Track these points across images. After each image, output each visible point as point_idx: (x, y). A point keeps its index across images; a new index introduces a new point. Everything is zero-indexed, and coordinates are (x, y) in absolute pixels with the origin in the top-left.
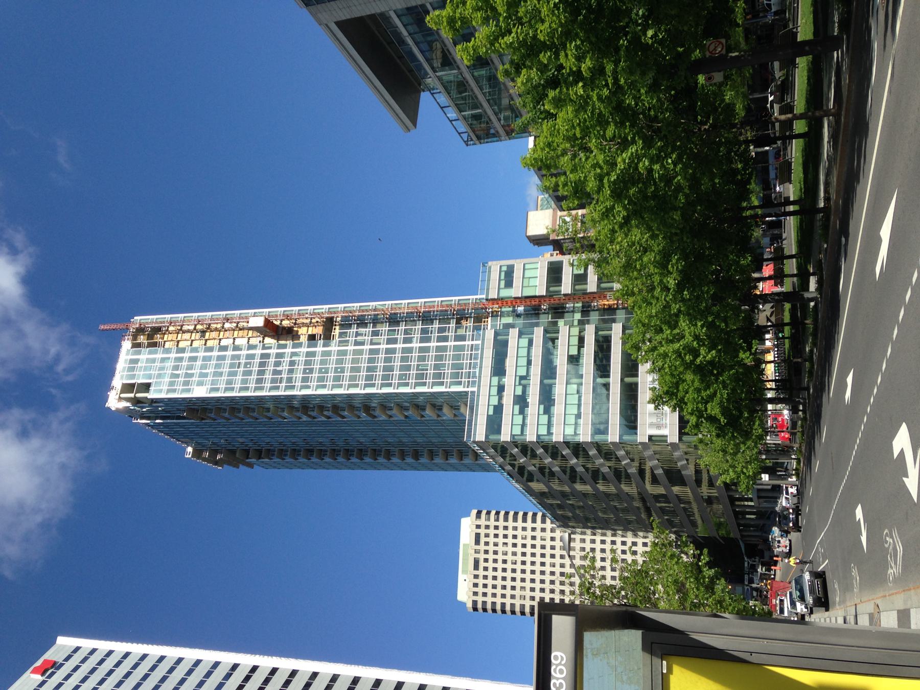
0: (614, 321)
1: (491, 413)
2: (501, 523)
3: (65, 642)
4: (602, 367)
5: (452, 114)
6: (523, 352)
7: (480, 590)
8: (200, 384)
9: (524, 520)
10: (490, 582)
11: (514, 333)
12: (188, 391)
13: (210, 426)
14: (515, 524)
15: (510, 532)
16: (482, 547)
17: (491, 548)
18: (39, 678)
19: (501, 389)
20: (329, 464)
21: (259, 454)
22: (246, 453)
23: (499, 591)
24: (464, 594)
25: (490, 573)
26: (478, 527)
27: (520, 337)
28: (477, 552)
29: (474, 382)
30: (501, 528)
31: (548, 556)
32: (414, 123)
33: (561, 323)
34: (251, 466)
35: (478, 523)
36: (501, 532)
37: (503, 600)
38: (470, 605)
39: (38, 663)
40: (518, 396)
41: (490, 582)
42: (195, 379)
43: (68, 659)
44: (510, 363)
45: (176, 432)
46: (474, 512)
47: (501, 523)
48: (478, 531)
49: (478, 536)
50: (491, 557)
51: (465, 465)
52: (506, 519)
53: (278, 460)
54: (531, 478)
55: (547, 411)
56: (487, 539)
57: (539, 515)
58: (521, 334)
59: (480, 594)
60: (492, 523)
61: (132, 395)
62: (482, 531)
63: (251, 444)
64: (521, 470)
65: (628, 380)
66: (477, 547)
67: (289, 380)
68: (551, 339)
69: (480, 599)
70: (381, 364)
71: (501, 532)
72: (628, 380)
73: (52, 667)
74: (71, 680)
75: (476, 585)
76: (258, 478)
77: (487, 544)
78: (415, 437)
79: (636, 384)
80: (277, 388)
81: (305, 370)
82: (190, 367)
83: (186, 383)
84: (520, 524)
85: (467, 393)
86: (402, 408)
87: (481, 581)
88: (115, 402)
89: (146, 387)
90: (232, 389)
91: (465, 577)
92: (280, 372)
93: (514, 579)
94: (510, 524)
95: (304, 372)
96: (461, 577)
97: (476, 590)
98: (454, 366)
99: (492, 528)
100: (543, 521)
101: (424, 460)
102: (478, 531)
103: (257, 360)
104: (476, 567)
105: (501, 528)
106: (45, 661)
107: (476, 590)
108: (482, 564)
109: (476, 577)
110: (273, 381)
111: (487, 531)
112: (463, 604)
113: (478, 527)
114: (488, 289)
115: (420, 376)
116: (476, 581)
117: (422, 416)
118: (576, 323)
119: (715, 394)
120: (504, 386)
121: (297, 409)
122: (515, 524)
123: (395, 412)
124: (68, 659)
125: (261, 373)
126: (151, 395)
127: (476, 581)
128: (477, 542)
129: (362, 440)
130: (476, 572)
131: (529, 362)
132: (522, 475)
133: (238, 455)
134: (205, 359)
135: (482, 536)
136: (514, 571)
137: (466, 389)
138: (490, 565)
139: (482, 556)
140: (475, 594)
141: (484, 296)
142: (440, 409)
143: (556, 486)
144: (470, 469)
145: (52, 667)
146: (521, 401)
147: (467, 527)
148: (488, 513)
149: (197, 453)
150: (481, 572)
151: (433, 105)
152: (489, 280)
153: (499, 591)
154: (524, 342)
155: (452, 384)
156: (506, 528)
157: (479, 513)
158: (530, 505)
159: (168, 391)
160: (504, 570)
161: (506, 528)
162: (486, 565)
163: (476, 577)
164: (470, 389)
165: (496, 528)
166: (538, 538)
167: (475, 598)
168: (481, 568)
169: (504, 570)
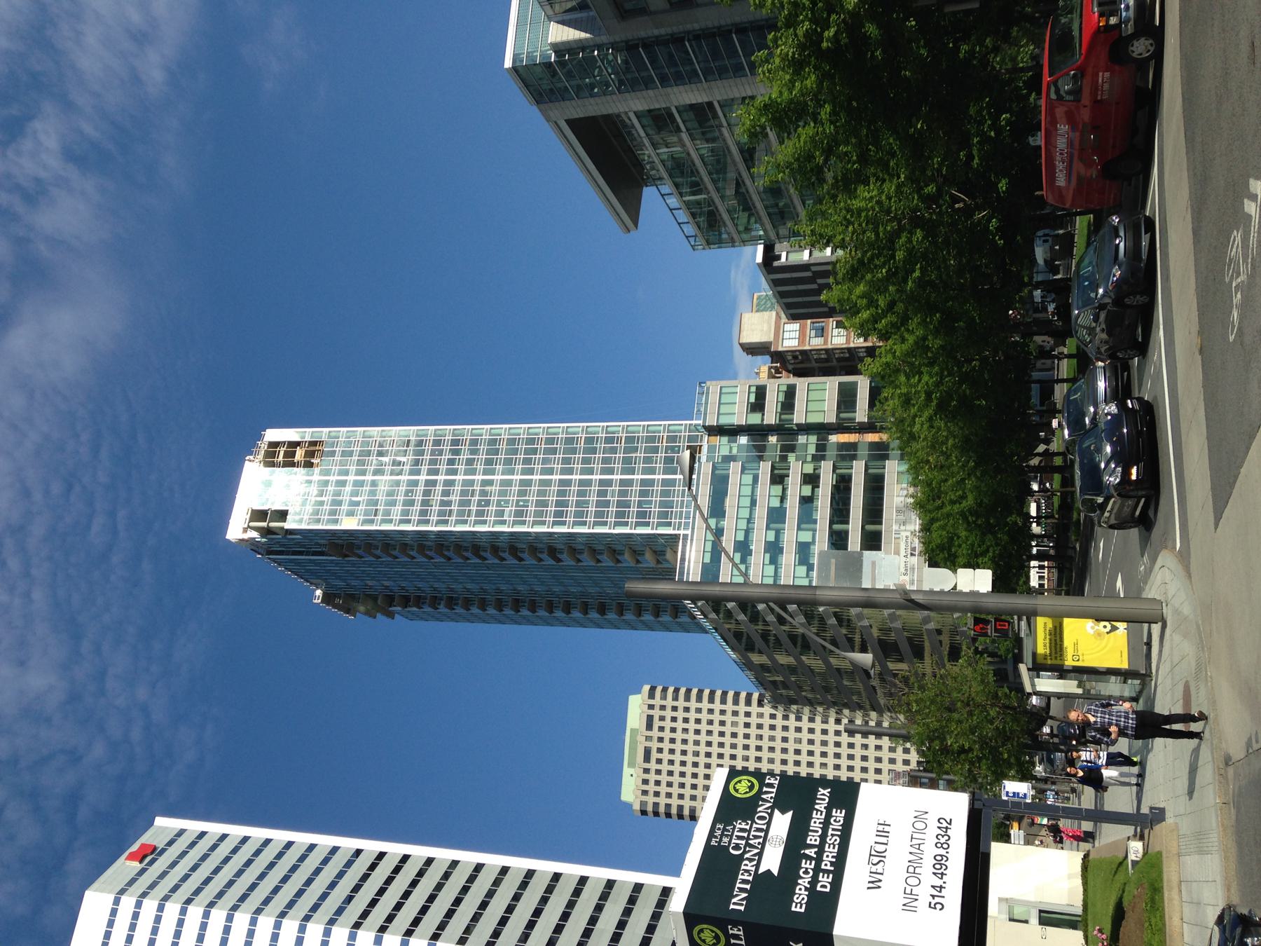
0: (854, 457)
1: (707, 560)
2: (681, 703)
3: (165, 824)
4: (840, 511)
5: (673, 201)
6: (747, 491)
7: (651, 788)
8: (351, 514)
9: (711, 700)
10: (664, 778)
11: (735, 468)
12: (336, 521)
13: (354, 565)
14: (699, 705)
15: (692, 715)
16: (655, 733)
17: (667, 735)
18: (136, 865)
19: (719, 533)
20: (492, 617)
21: (406, 601)
22: (390, 600)
23: (675, 790)
24: (629, 791)
25: (665, 767)
26: (651, 707)
27: (742, 472)
28: (648, 738)
29: (687, 524)
30: (681, 710)
31: (740, 747)
32: (636, 223)
33: (792, 458)
34: (391, 615)
35: (651, 702)
36: (680, 715)
37: (681, 802)
38: (637, 807)
39: (135, 848)
40: (740, 542)
41: (664, 778)
42: (345, 507)
43: (170, 843)
44: (730, 503)
45: (307, 571)
46: (646, 688)
47: (681, 703)
48: (651, 712)
49: (650, 719)
50: (666, 746)
51: (680, 624)
52: (687, 699)
53: (430, 609)
54: (750, 647)
55: (774, 561)
56: (662, 724)
57: (756, 696)
58: (743, 470)
59: (651, 793)
60: (669, 702)
61: (264, 524)
62: (656, 713)
63: (396, 589)
64: (738, 635)
65: (870, 527)
66: (649, 733)
67: (387, 513)
68: (778, 479)
69: (651, 799)
70: (573, 499)
71: (680, 715)
72: (870, 527)
73: (148, 854)
74: (177, 868)
75: (645, 782)
76: (403, 630)
77: (661, 729)
78: (595, 585)
79: (847, 532)
80: (446, 522)
81: (518, 501)
82: (338, 494)
83: (333, 513)
84: (705, 705)
85: (676, 537)
86: (594, 552)
87: (652, 777)
88: (238, 528)
89: (283, 515)
90: (427, 522)
91: (632, 771)
92: (449, 503)
93: (658, 783)
94: (693, 704)
95: (479, 504)
96: (627, 771)
97: (645, 787)
98: (662, 504)
99: (669, 709)
100: (760, 704)
101: (612, 616)
102: (651, 712)
103: (421, 488)
104: (647, 758)
105: (681, 710)
106: (143, 846)
107: (645, 787)
108: (655, 755)
109: (646, 771)
110: (441, 513)
111: (663, 713)
112: (628, 806)
113: (651, 707)
114: (705, 414)
115: (642, 515)
116: (646, 776)
117: (638, 562)
118: (809, 458)
119: (987, 551)
120: (723, 530)
121: (430, 549)
122: (699, 705)
123: (604, 557)
124: (170, 843)
125: (425, 503)
126: (289, 524)
127: (646, 776)
128: (649, 726)
129: (520, 588)
130: (647, 766)
131: (753, 503)
132: (741, 642)
133: (388, 602)
134: (356, 483)
135: (656, 719)
136: (695, 765)
137: (676, 532)
138: (666, 756)
139: (655, 745)
140: (645, 793)
141: (701, 422)
142: (642, 554)
143: (783, 659)
144: (687, 630)
145: (148, 854)
146: (743, 548)
147: (636, 707)
148: (665, 690)
149: (327, 598)
150: (653, 766)
151: (658, 203)
152: (706, 403)
153: (675, 790)
154: (748, 479)
155: (659, 524)
156: (699, 710)
157: (653, 689)
158: (745, 683)
159: (365, 522)
160: (683, 763)
161: (687, 710)
162: (660, 756)
163: (646, 771)
164: (682, 532)
165: (675, 709)
166: (728, 724)
167: (644, 798)
168: (653, 760)
169: (658, 772)
